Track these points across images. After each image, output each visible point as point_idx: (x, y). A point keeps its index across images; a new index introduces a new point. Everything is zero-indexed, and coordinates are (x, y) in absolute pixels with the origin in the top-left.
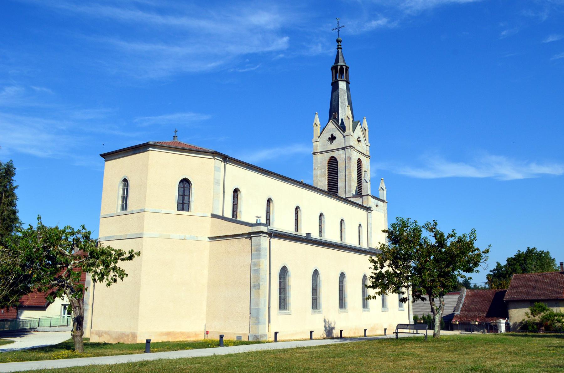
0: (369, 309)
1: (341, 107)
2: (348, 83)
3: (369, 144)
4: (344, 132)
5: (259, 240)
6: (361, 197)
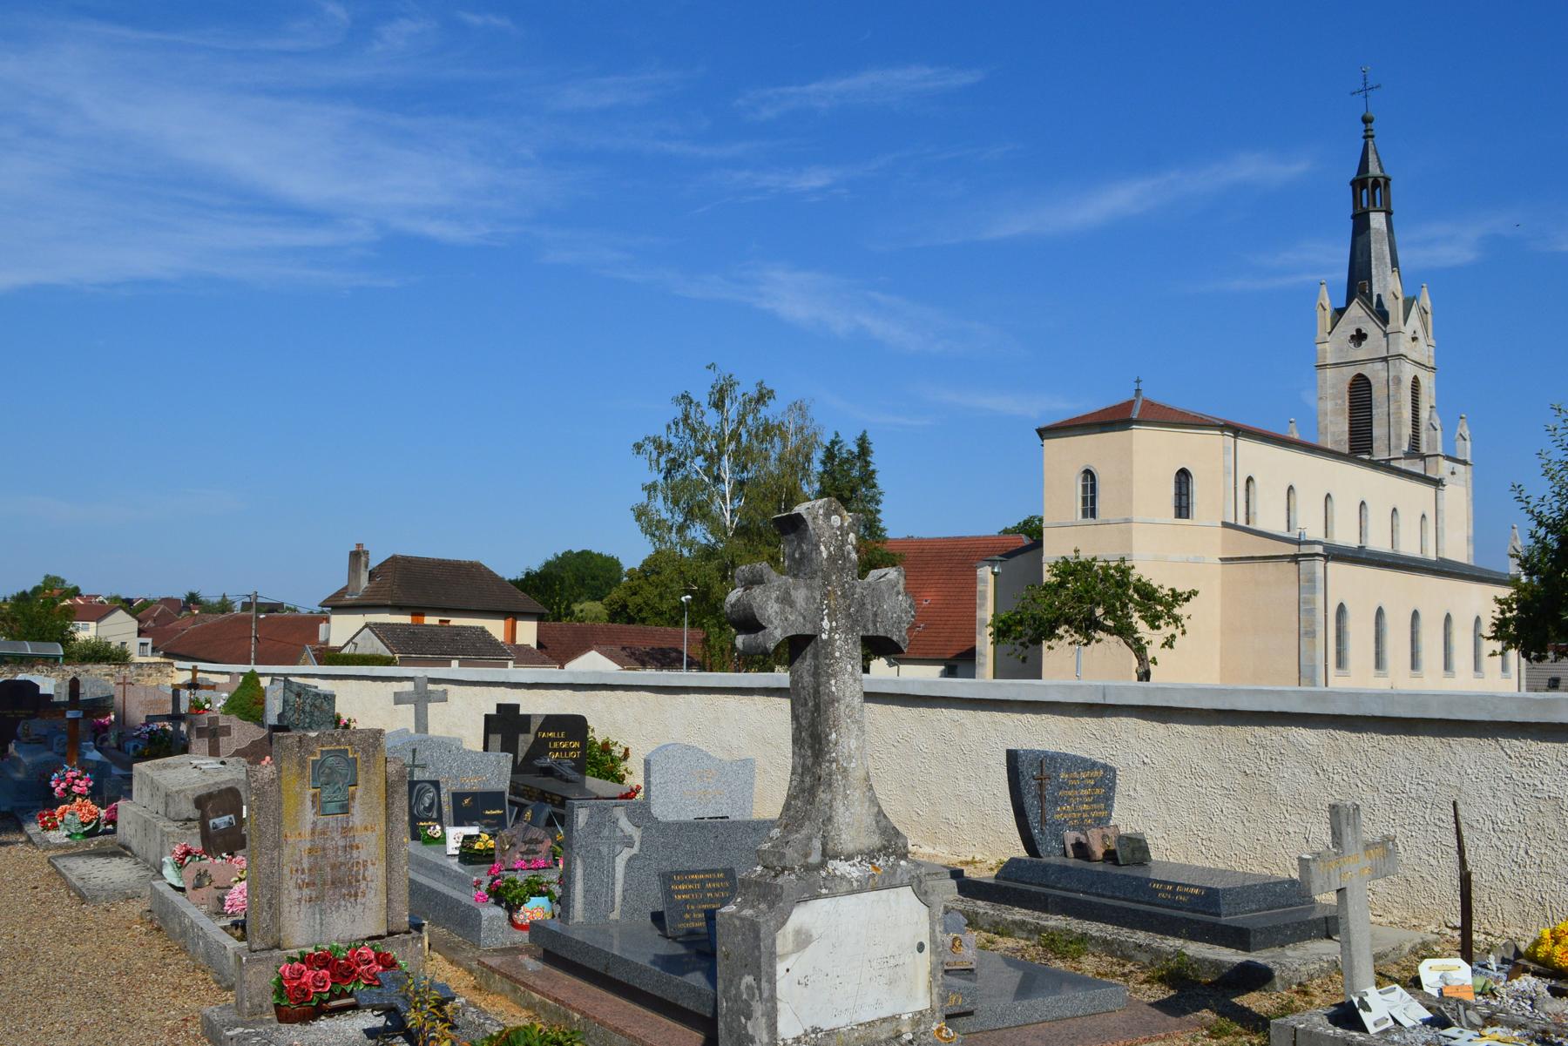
0: (1454, 672)
1: (1376, 268)
2: (1389, 213)
3: (1433, 342)
4: (1385, 326)
5: (1314, 566)
6: (1423, 457)
